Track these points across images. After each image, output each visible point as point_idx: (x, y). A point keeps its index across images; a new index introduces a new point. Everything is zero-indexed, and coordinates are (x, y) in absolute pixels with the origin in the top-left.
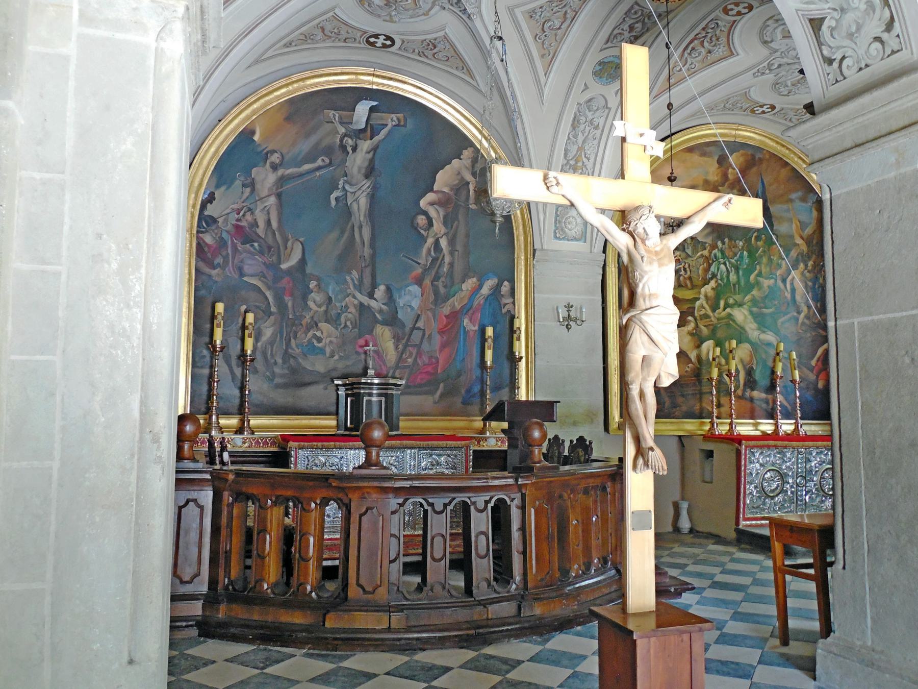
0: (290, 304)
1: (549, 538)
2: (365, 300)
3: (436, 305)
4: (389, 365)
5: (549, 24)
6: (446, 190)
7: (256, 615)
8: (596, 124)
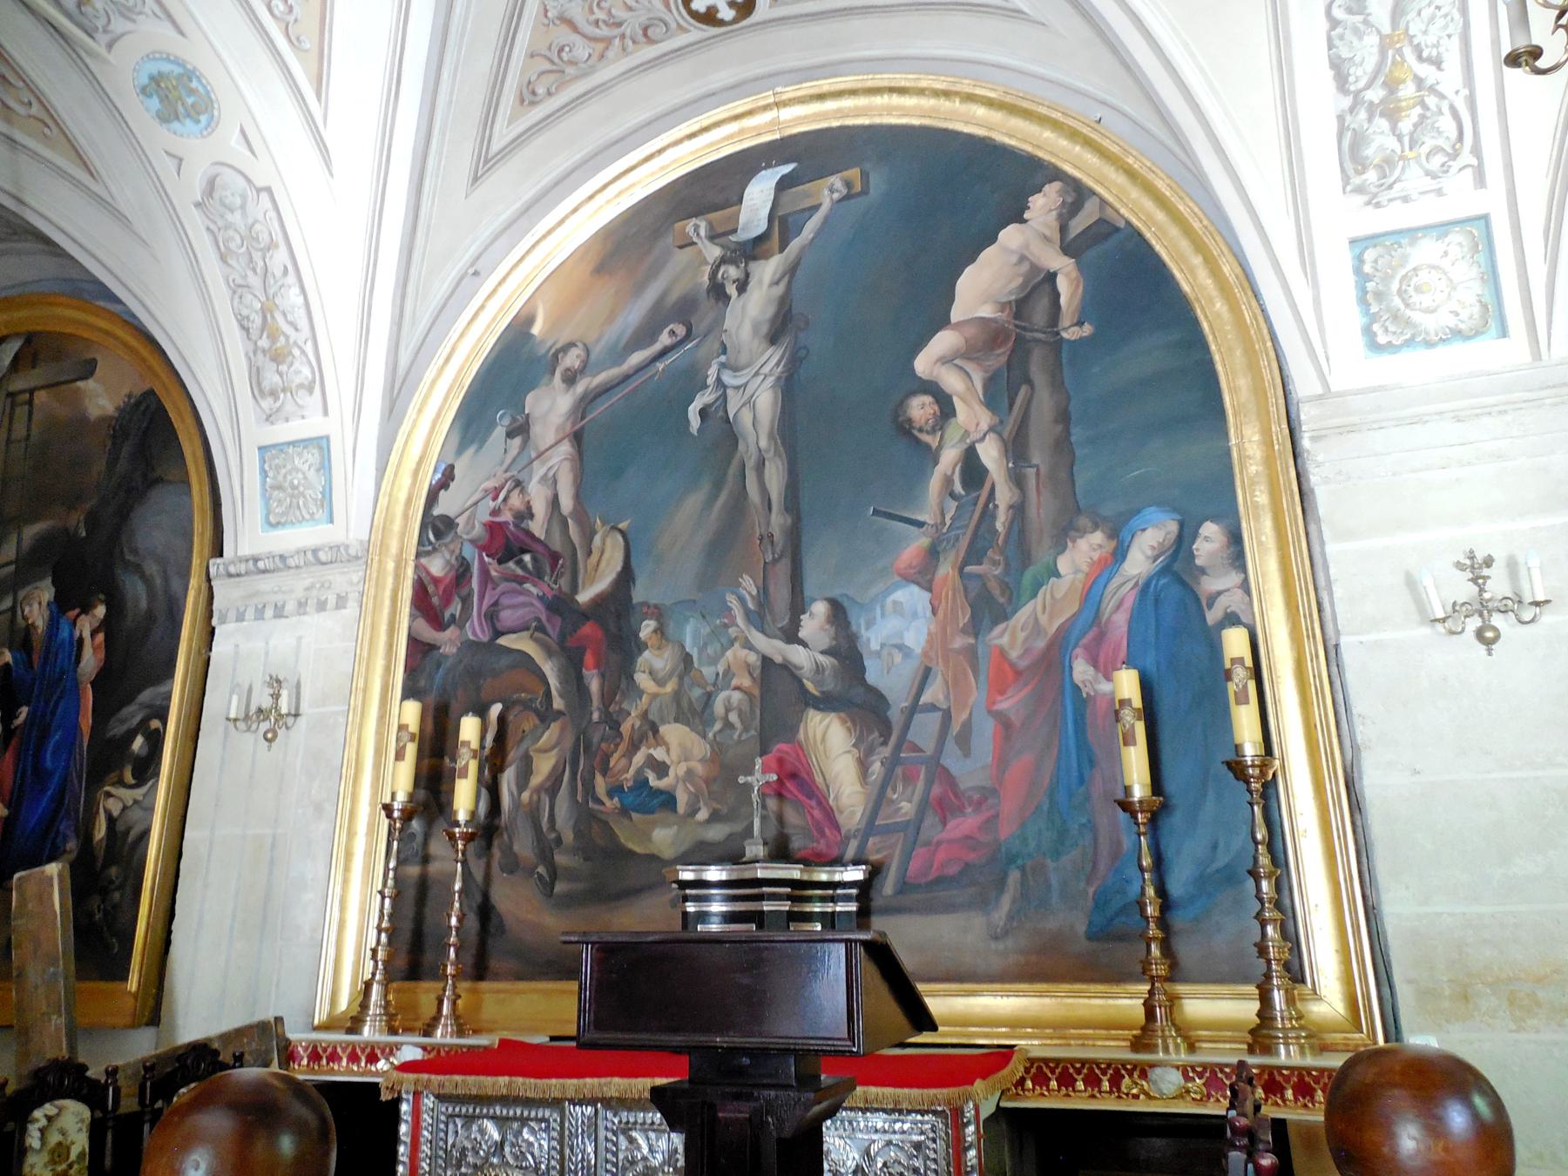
2: (776, 648)
3: (976, 636)
6: (987, 312)
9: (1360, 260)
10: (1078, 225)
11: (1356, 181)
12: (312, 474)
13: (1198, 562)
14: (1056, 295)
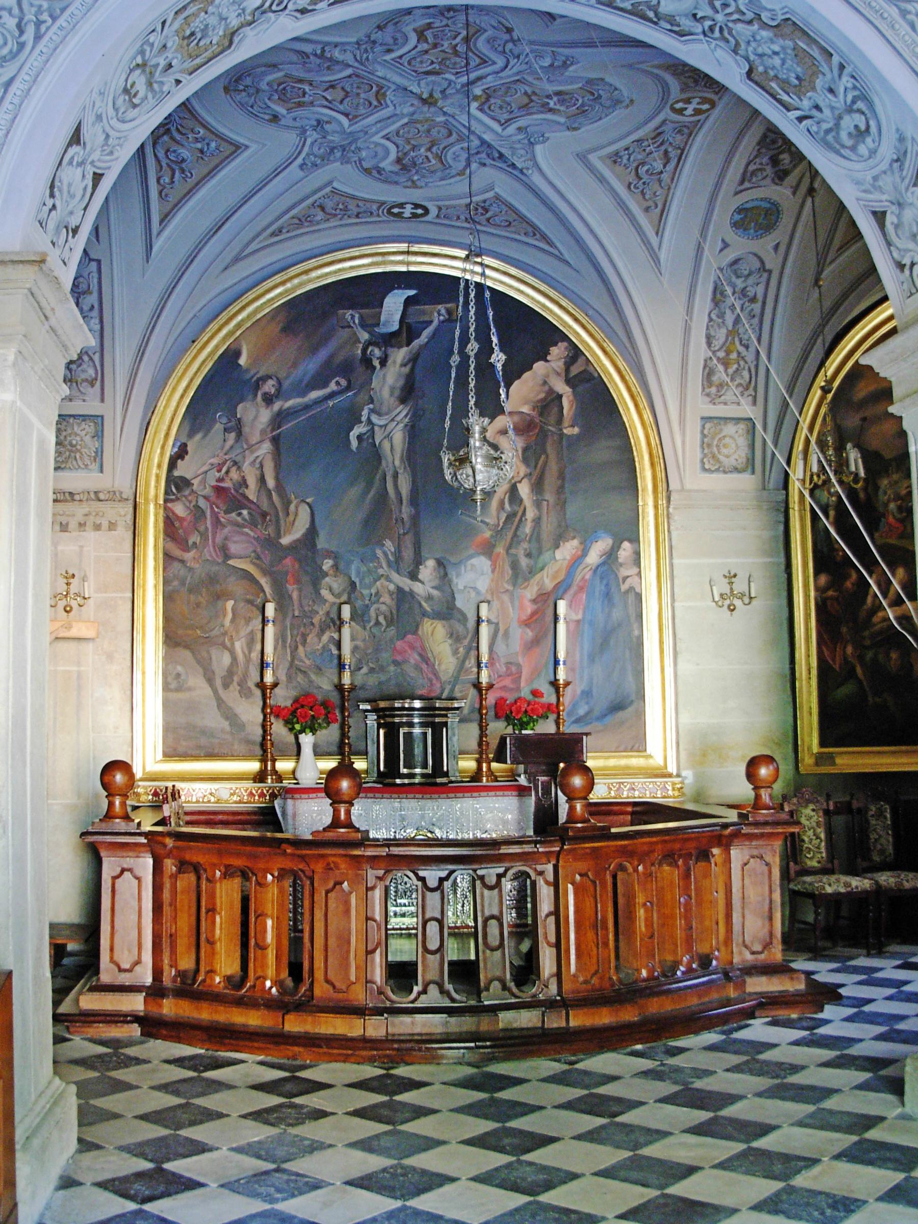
0: (295, 595)
1: (598, 925)
2: (406, 583)
3: (514, 585)
4: (443, 679)
5: (646, 168)
6: (525, 409)
7: (205, 1014)
8: (751, 294)
9: (703, 427)
10: (575, 370)
11: (707, 390)
12: (87, 439)
13: (620, 560)
14: (561, 408)
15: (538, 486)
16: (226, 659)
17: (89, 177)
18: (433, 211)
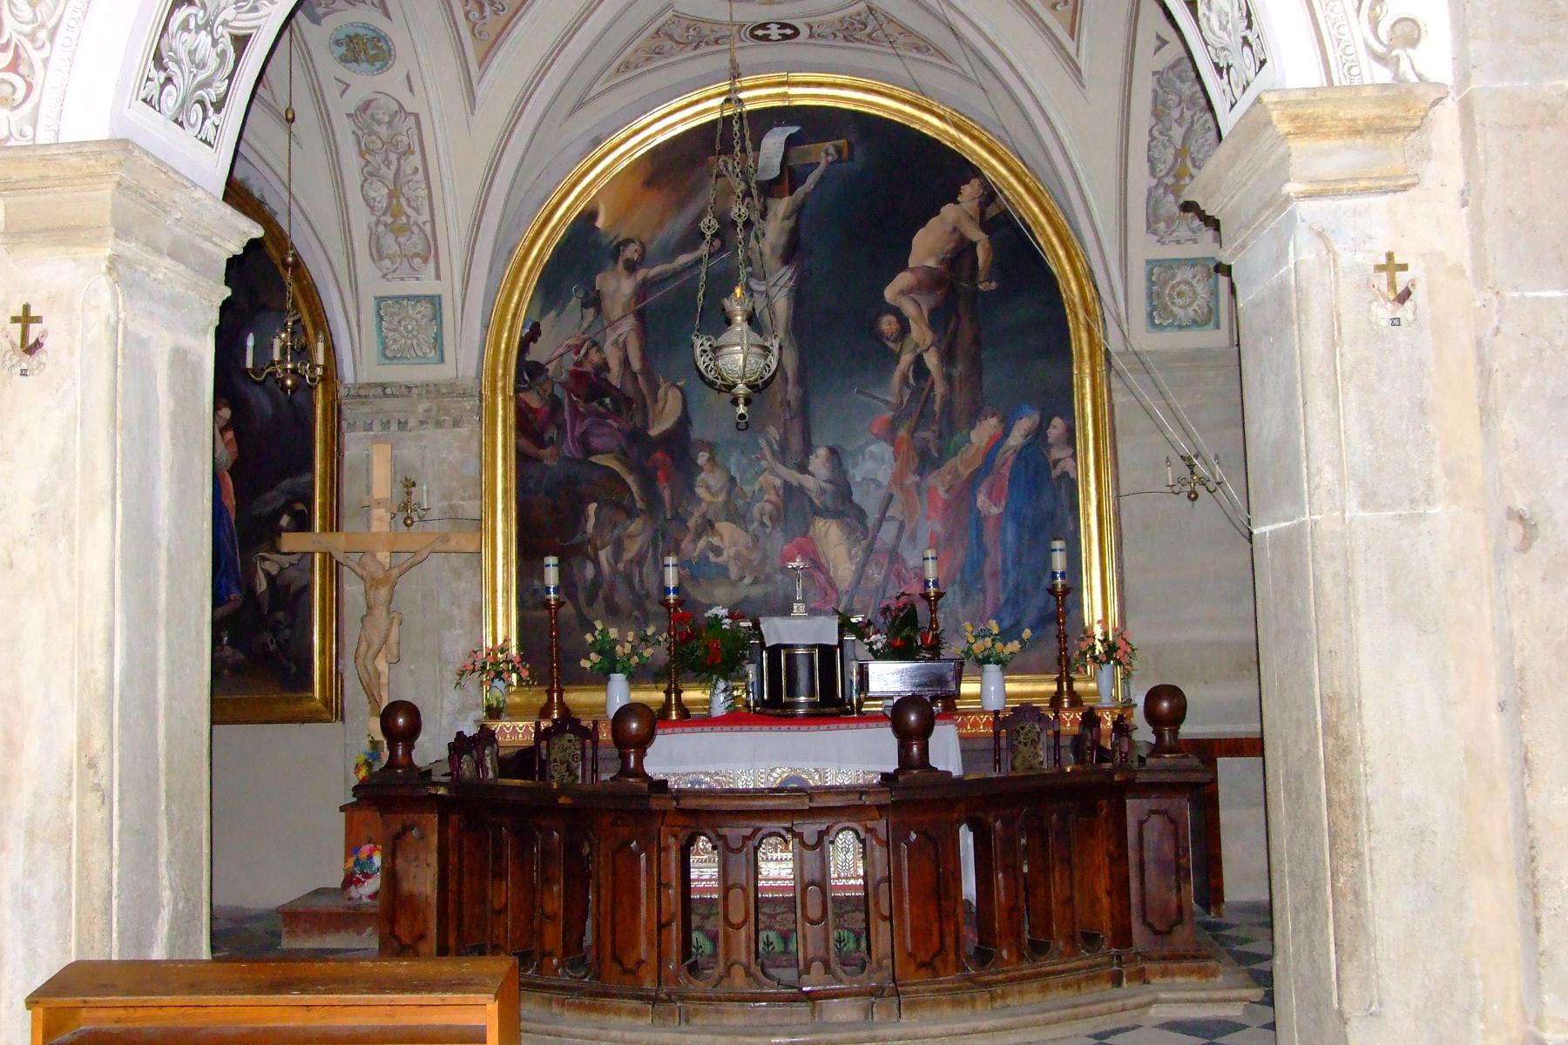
0: (666, 494)
2: (794, 477)
3: (921, 475)
6: (931, 263)
9: (1150, 273)
10: (992, 211)
15: (948, 357)
16: (590, 571)
17: (226, 44)
18: (804, 31)
